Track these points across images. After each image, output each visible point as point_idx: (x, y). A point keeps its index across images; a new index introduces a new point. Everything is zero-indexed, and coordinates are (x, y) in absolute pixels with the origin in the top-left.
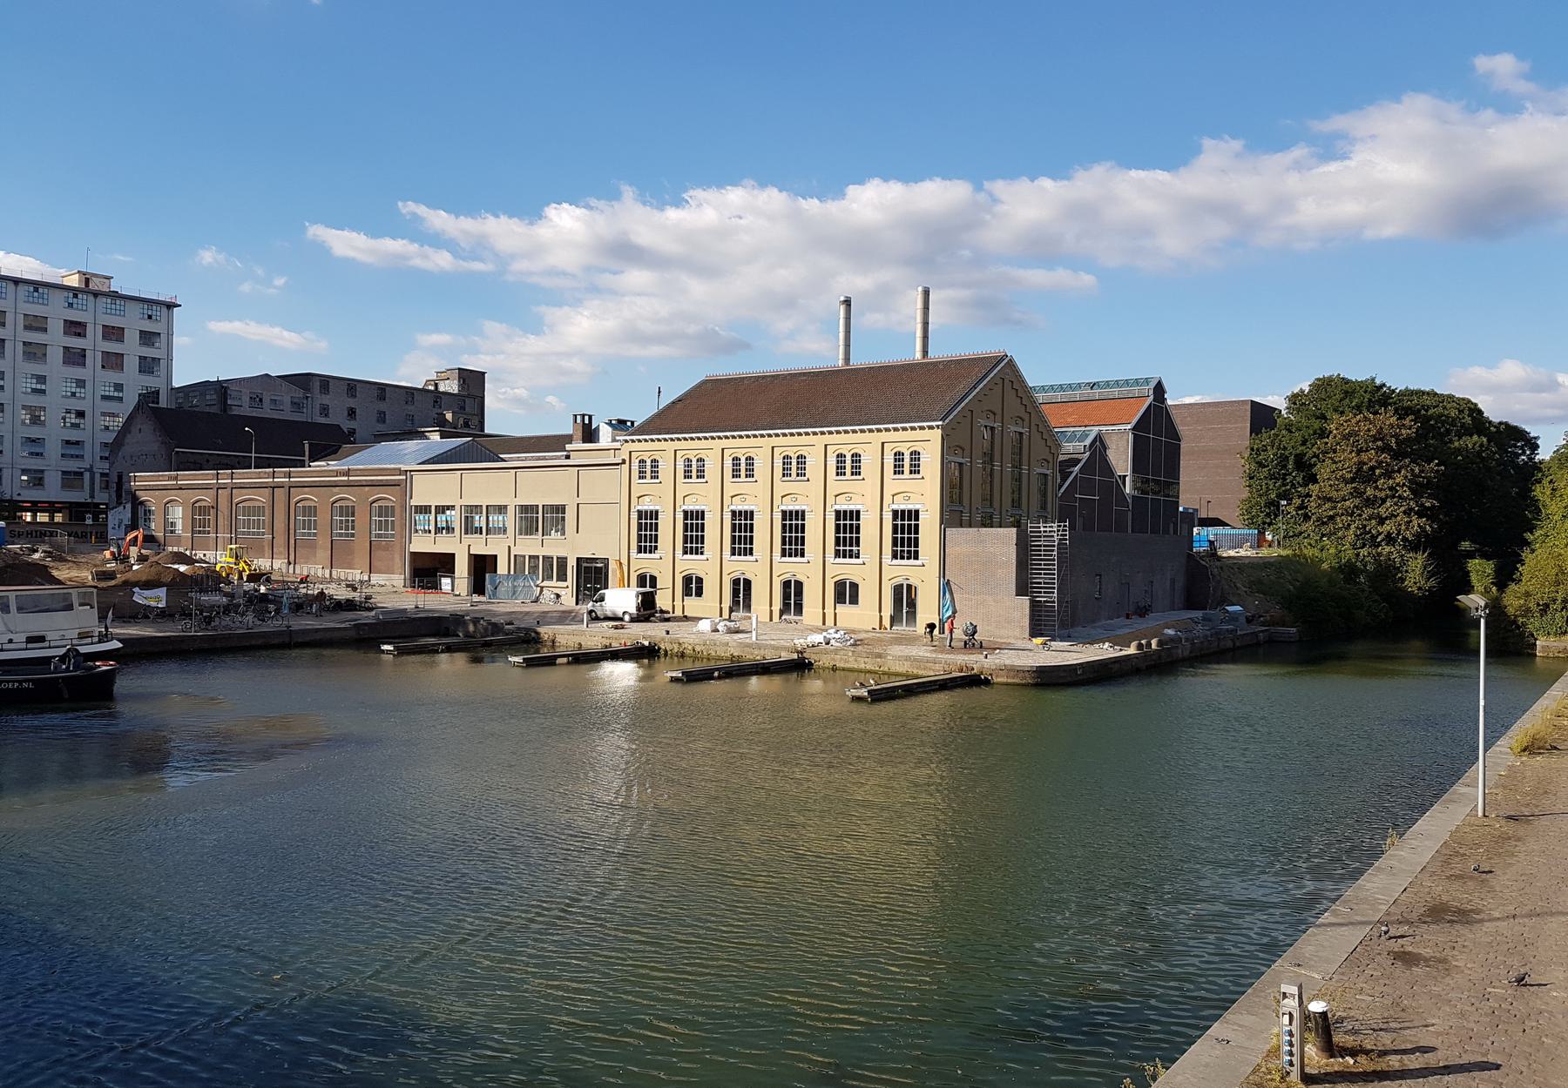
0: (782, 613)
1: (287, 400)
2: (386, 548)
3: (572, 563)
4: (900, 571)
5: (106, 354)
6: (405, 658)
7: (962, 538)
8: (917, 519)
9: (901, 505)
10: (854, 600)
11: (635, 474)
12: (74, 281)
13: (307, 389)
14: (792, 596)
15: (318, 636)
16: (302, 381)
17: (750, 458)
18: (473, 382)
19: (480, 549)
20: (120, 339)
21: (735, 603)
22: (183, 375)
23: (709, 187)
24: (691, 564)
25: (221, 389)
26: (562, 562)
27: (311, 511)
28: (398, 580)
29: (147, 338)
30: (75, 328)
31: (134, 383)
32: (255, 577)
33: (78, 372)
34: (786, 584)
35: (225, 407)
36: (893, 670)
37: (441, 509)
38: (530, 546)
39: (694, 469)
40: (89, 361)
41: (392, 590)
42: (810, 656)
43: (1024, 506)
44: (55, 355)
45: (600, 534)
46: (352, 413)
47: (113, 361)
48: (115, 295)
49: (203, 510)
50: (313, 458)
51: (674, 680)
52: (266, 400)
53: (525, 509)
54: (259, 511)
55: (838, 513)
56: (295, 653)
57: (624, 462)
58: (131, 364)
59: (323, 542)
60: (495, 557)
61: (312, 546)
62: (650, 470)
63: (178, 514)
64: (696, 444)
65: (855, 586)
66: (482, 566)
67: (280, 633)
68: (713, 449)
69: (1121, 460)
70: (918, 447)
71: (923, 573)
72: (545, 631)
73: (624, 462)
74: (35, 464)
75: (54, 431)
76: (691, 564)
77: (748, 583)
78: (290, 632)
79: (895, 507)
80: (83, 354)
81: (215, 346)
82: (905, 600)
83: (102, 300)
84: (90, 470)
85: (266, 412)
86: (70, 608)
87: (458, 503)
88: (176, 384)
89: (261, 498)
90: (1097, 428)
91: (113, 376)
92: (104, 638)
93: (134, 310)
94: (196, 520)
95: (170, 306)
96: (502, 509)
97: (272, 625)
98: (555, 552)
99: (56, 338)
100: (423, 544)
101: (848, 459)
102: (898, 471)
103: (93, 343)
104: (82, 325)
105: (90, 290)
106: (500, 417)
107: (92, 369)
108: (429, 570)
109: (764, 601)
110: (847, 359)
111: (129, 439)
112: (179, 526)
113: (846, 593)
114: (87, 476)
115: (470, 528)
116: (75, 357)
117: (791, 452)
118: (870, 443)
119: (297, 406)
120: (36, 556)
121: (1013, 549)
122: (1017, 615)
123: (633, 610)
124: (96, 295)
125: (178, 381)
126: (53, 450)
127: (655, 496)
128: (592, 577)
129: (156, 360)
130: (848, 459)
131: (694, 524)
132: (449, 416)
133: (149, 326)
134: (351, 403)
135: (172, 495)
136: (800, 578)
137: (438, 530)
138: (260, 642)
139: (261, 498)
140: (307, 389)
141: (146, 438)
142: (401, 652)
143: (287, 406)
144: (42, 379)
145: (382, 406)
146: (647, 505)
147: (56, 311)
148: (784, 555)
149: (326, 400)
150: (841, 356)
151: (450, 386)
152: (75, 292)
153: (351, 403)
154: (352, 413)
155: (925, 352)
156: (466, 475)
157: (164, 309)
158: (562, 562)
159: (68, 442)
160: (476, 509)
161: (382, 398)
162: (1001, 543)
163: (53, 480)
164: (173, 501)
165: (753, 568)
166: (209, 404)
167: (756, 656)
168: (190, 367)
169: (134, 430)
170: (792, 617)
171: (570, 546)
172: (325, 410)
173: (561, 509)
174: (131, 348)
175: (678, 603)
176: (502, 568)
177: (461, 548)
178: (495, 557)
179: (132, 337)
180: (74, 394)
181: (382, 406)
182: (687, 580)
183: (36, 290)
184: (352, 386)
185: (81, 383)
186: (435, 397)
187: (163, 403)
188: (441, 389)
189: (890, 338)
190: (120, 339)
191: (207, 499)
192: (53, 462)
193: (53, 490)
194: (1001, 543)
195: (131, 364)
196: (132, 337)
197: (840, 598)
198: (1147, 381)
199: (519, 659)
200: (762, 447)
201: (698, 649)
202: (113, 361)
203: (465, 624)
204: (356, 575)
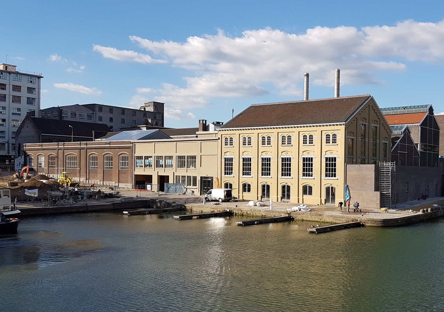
0: (282, 198)
1: (86, 114)
2: (125, 173)
3: (198, 179)
4: (329, 182)
5: (14, 96)
7: (354, 169)
8: (335, 161)
10: (310, 193)
11: (224, 143)
14: (286, 192)
15: (98, 208)
17: (269, 137)
20: (20, 90)
21: (263, 194)
23: (253, 30)
25: (59, 110)
27: (95, 158)
29: (30, 90)
31: (25, 108)
32: (73, 185)
35: (61, 117)
36: (326, 221)
37: (147, 158)
38: (182, 172)
41: (127, 190)
42: (293, 215)
45: (210, 167)
46: (111, 120)
47: (17, 99)
48: (17, 73)
49: (53, 158)
50: (96, 137)
51: (239, 225)
53: (180, 157)
54: (75, 158)
57: (219, 139)
58: (24, 100)
59: (100, 171)
61: (96, 172)
63: (42, 160)
64: (287, 130)
65: (311, 188)
66: (163, 180)
67: (83, 207)
68: (254, 133)
69: (416, 137)
70: (335, 132)
72: (188, 206)
73: (219, 139)
78: (87, 207)
79: (262, 157)
81: (55, 94)
82: (330, 193)
83: (12, 75)
85: (77, 119)
87: (175, 155)
88: (42, 108)
90: (406, 125)
91: (17, 105)
92: (13, 209)
93: (25, 79)
94: (49, 162)
95: (39, 77)
96: (171, 158)
97: (80, 204)
100: (139, 171)
101: (266, 138)
102: (328, 141)
106: (170, 121)
109: (275, 193)
111: (23, 130)
112: (43, 165)
113: (307, 190)
114: (6, 145)
115: (158, 165)
118: (317, 131)
119: (89, 117)
123: (223, 197)
124: (10, 73)
127: (231, 152)
128: (207, 184)
129: (34, 99)
130: (266, 138)
131: (247, 163)
133: (31, 85)
134: (111, 116)
136: (289, 184)
138: (75, 210)
141: (30, 130)
142: (131, 214)
143: (86, 117)
145: (123, 117)
146: (228, 156)
149: (101, 114)
151: (150, 109)
153: (111, 116)
154: (111, 120)
155: (338, 95)
157: (37, 79)
158: (195, 178)
160: (160, 157)
162: (368, 170)
164: (41, 155)
167: (272, 215)
168: (48, 100)
169: (25, 126)
170: (286, 200)
172: (101, 119)
173: (194, 157)
174: (24, 94)
175: (241, 194)
176: (171, 181)
177: (155, 173)
179: (24, 90)
181: (123, 117)
182: (244, 185)
184: (111, 109)
187: (36, 116)
190: (20, 90)
191: (54, 154)
194: (368, 170)
195: (24, 100)
196: (24, 90)
197: (305, 192)
198: (426, 106)
199: (178, 217)
200: (274, 133)
201: (248, 212)
202: (17, 99)
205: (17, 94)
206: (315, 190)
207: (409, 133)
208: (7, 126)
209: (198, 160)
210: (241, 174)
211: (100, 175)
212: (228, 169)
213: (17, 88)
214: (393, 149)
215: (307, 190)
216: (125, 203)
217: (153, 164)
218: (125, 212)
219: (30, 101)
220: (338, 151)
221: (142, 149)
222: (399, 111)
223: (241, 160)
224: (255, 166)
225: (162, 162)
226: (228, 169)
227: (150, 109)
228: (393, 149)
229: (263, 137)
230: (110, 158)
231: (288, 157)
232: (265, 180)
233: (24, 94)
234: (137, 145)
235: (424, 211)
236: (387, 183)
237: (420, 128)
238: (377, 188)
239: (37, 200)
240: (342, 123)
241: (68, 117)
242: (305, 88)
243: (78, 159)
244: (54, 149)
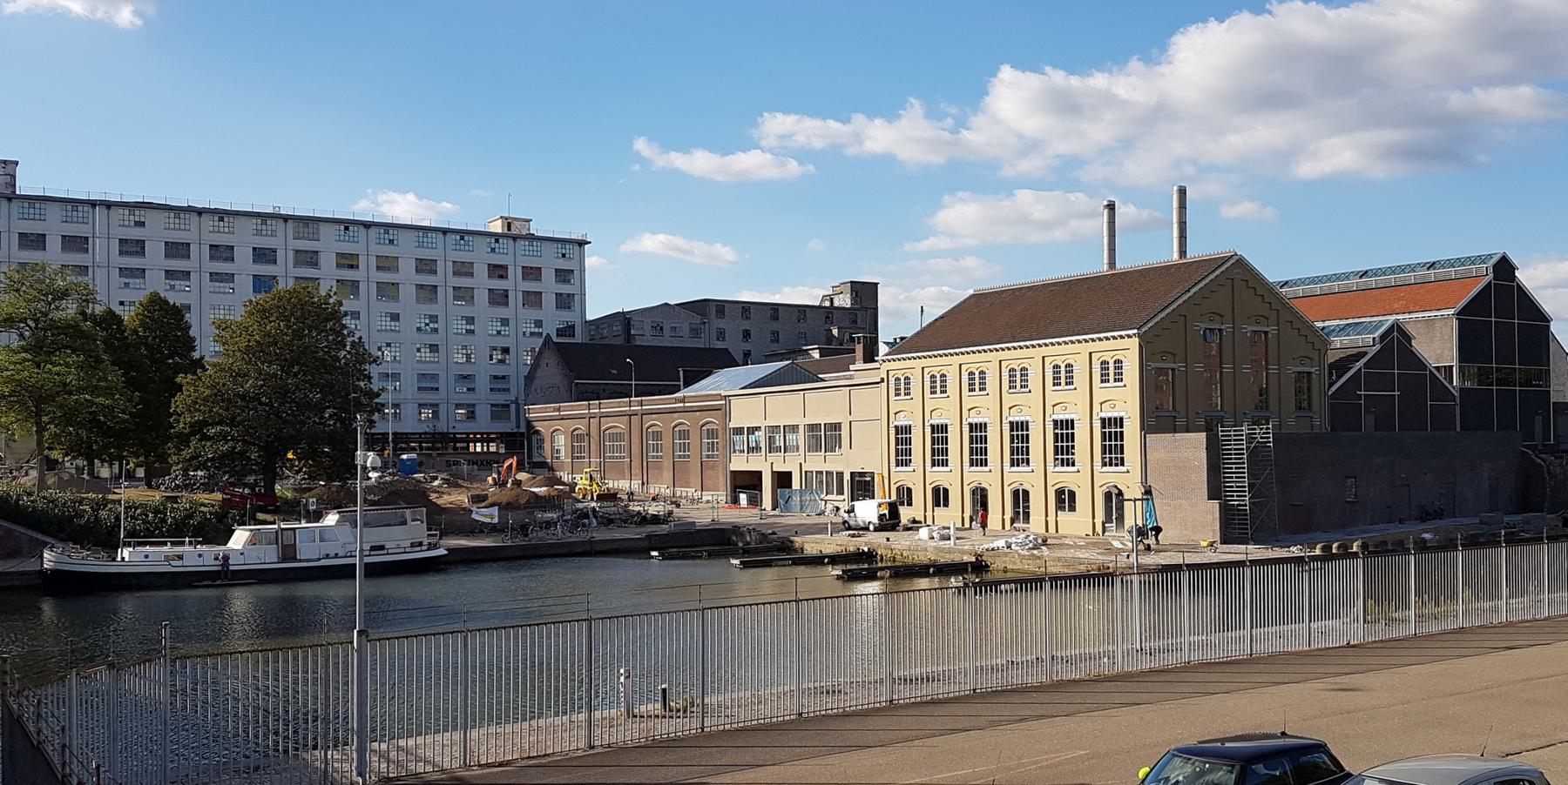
0: (1013, 521)
1: (686, 327)
2: (713, 468)
3: (847, 477)
4: (1109, 477)
5: (526, 293)
6: (906, 585)
7: (1161, 443)
11: (1049, 381)
12: (497, 227)
13: (704, 315)
15: (615, 546)
16: (699, 307)
18: (865, 293)
19: (780, 467)
21: (1108, 519)
22: (597, 306)
24: (1063, 477)
25: (624, 320)
26: (840, 475)
27: (658, 436)
28: (722, 496)
32: (611, 496)
33: (501, 312)
37: (752, 430)
39: (1111, 371)
41: (708, 506)
42: (987, 559)
44: (482, 297)
45: (866, 452)
46: (747, 335)
47: (533, 299)
48: (532, 238)
49: (580, 438)
50: (687, 385)
52: (666, 328)
53: (813, 428)
54: (617, 437)
56: (547, 561)
58: (549, 301)
59: (667, 464)
60: (760, 473)
61: (659, 466)
63: (561, 441)
67: (584, 543)
68: (990, 360)
70: (984, 367)
71: (1128, 479)
72: (798, 540)
74: (469, 399)
75: (484, 369)
76: (1063, 477)
78: (591, 542)
79: (1103, 415)
80: (505, 294)
81: (628, 276)
82: (1114, 501)
85: (667, 341)
86: (404, 523)
87: (802, 422)
88: (589, 317)
90: (1394, 317)
91: (535, 314)
92: (431, 547)
93: (550, 250)
94: (589, 449)
95: (582, 243)
96: (794, 428)
97: (580, 536)
98: (834, 468)
99: (482, 282)
100: (739, 463)
101: (1111, 365)
102: (1100, 377)
103: (515, 284)
104: (504, 268)
108: (747, 482)
110: (1112, 264)
111: (539, 373)
112: (563, 453)
113: (1065, 500)
114: (513, 407)
116: (499, 298)
117: (935, 371)
118: (1076, 351)
119: (695, 332)
120: (436, 483)
121: (1203, 455)
122: (1209, 517)
123: (876, 521)
124: (515, 238)
125: (591, 315)
126: (483, 384)
127: (909, 413)
128: (862, 486)
130: (1111, 365)
131: (1064, 433)
132: (835, 332)
133: (563, 265)
134: (746, 325)
135: (557, 425)
136: (1026, 487)
138: (565, 550)
139: (621, 425)
140: (704, 315)
141: (552, 372)
145: (776, 326)
146: (902, 421)
147: (481, 257)
148: (1104, 464)
149: (721, 324)
150: (1106, 261)
151: (844, 301)
152: (497, 237)
154: (747, 335)
155: (1183, 253)
156: (769, 398)
158: (840, 475)
159: (495, 377)
161: (775, 318)
162: (1192, 447)
163: (483, 412)
164: (560, 426)
165: (1028, 478)
166: (615, 337)
167: (923, 558)
168: (602, 299)
169: (543, 364)
171: (844, 462)
172: (721, 335)
173: (836, 427)
174: (549, 286)
175: (929, 513)
176: (796, 485)
178: (760, 473)
179: (548, 276)
180: (499, 332)
181: (776, 326)
182: (1060, 493)
183: (462, 238)
184: (746, 308)
185: (505, 322)
186: (827, 313)
188: (836, 304)
189: (1066, 249)
190: (142, 253)
191: (582, 427)
192: (484, 396)
193: (484, 422)
194: (1192, 447)
195: (549, 301)
196: (548, 276)
197: (1060, 504)
198: (1483, 259)
199: (736, 562)
200: (1033, 356)
202: (533, 299)
203: (742, 535)
204: (664, 489)
205: (532, 286)
206: (1082, 501)
207: (1409, 339)
208: (513, 362)
211: (668, 475)
212: (903, 456)
213: (532, 273)
214: (1334, 388)
215: (1065, 500)
216: (682, 534)
217: (762, 445)
218: (654, 553)
219: (564, 302)
220: (1125, 401)
221: (745, 412)
222: (1411, 277)
224: (1040, 442)
226: (903, 456)
227: (844, 301)
228: (1334, 388)
230: (684, 435)
231: (1116, 414)
232: (976, 476)
234: (734, 401)
235: (1323, 549)
237: (1455, 323)
238: (1215, 492)
239: (493, 529)
240: (1130, 332)
242: (1176, 233)
243: (627, 437)
244: (581, 417)
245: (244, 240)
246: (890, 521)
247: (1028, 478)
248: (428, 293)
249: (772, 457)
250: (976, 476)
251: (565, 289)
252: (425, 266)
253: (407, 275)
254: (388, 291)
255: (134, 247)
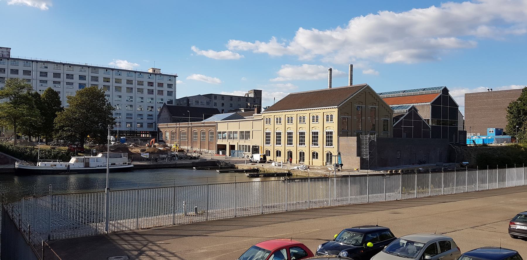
0: (299, 161)
1: (205, 102)
2: (212, 143)
3: (251, 147)
4: (328, 149)
5: (159, 91)
6: (268, 179)
7: (343, 139)
9: (277, 131)
12: (151, 71)
15: (183, 165)
16: (209, 96)
17: (317, 116)
18: (258, 93)
21: (327, 161)
23: (411, 9)
25: (187, 99)
27: (196, 133)
28: (214, 152)
29: (170, 86)
30: (151, 84)
31: (166, 98)
32: (182, 151)
34: (300, 153)
35: (188, 104)
37: (224, 133)
38: (242, 142)
40: (154, 93)
43: (377, 129)
45: (257, 140)
47: (161, 92)
48: (161, 74)
49: (173, 134)
50: (205, 119)
51: (248, 176)
54: (185, 133)
55: (327, 132)
58: (165, 93)
59: (199, 142)
61: (196, 143)
62: (268, 121)
63: (168, 134)
64: (316, 111)
66: (232, 147)
68: (294, 114)
74: (141, 121)
77: (304, 153)
78: (176, 164)
82: (329, 156)
84: (155, 123)
86: (121, 157)
87: (238, 131)
88: (177, 98)
89: (185, 130)
91: (161, 97)
92: (129, 164)
94: (175, 137)
95: (175, 76)
96: (236, 132)
97: (173, 162)
98: (248, 144)
99: (146, 87)
100: (220, 142)
103: (155, 88)
104: (152, 83)
105: (156, 73)
107: (155, 95)
108: (222, 148)
110: (330, 86)
113: (315, 155)
114: (154, 124)
116: (151, 92)
117: (328, 114)
118: (319, 112)
119: (208, 103)
123: (259, 160)
124: (156, 75)
125: (178, 97)
126: (145, 117)
127: (270, 129)
129: (172, 92)
131: (315, 135)
132: (249, 104)
133: (170, 83)
134: (223, 102)
135: (167, 129)
136: (304, 151)
137: (223, 138)
139: (185, 130)
142: (221, 172)
143: (205, 103)
144: (142, 98)
145: (231, 102)
146: (268, 131)
147: (146, 80)
149: (216, 101)
151: (252, 95)
152: (150, 74)
153: (223, 102)
154: (223, 104)
155: (351, 84)
158: (249, 146)
160: (230, 132)
162: (352, 141)
163: (145, 125)
164: (167, 130)
167: (273, 171)
169: (163, 112)
171: (250, 142)
173: (249, 132)
174: (165, 89)
175: (275, 158)
176: (236, 149)
177: (227, 143)
179: (165, 86)
181: (231, 102)
182: (313, 153)
184: (223, 97)
185: (152, 99)
187: (174, 104)
193: (145, 128)
194: (352, 141)
195: (165, 93)
196: (165, 86)
198: (439, 88)
200: (306, 113)
202: (161, 92)
204: (198, 149)
205: (161, 89)
206: (320, 156)
207: (417, 111)
209: (251, 134)
210: (298, 144)
211: (199, 145)
212: (268, 142)
213: (161, 85)
215: (315, 155)
219: (170, 93)
220: (333, 127)
221: (222, 127)
222: (418, 93)
223: (298, 134)
224: (308, 138)
225: (232, 136)
226: (268, 142)
227: (252, 95)
229: (313, 116)
230: (204, 133)
233: (165, 89)
235: (390, 172)
236: (366, 151)
237: (430, 106)
238: (359, 154)
241: (193, 105)
245: (76, 73)
246: (263, 160)
247: (304, 148)
248: (130, 90)
249: (229, 141)
250: (289, 148)
251: (170, 90)
252: (129, 82)
253: (124, 85)
254: (118, 89)
255: (118, 81)
